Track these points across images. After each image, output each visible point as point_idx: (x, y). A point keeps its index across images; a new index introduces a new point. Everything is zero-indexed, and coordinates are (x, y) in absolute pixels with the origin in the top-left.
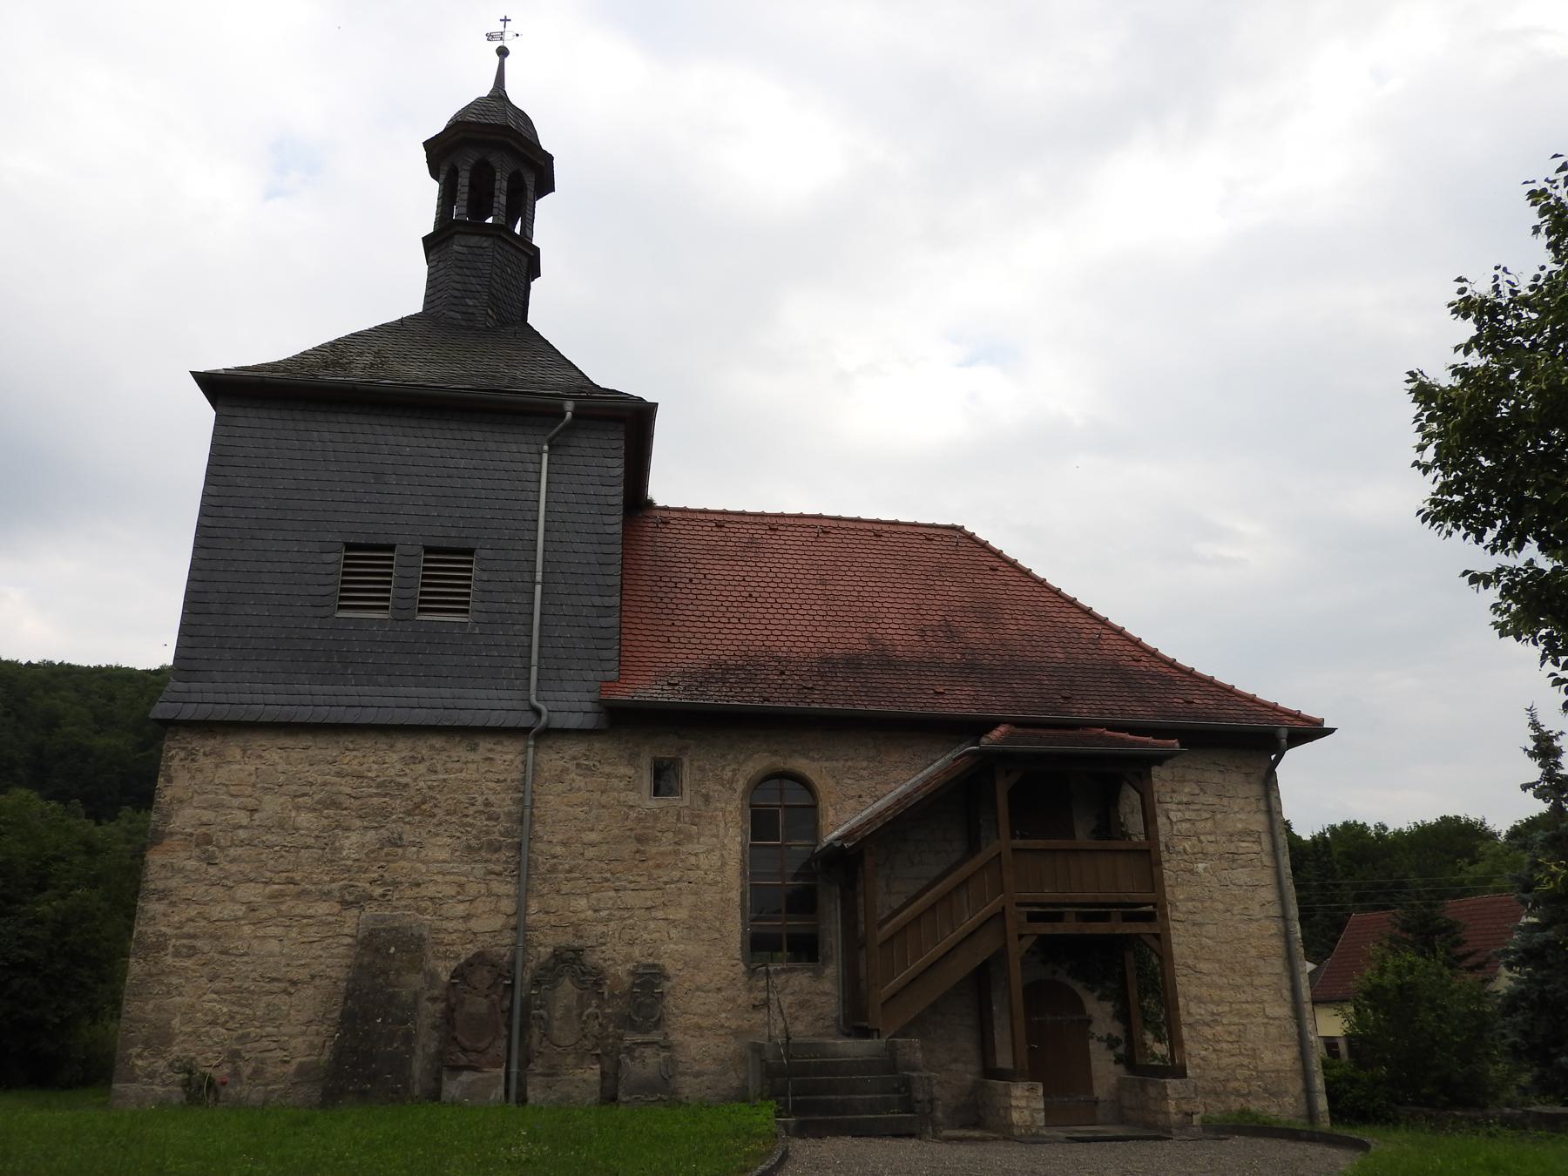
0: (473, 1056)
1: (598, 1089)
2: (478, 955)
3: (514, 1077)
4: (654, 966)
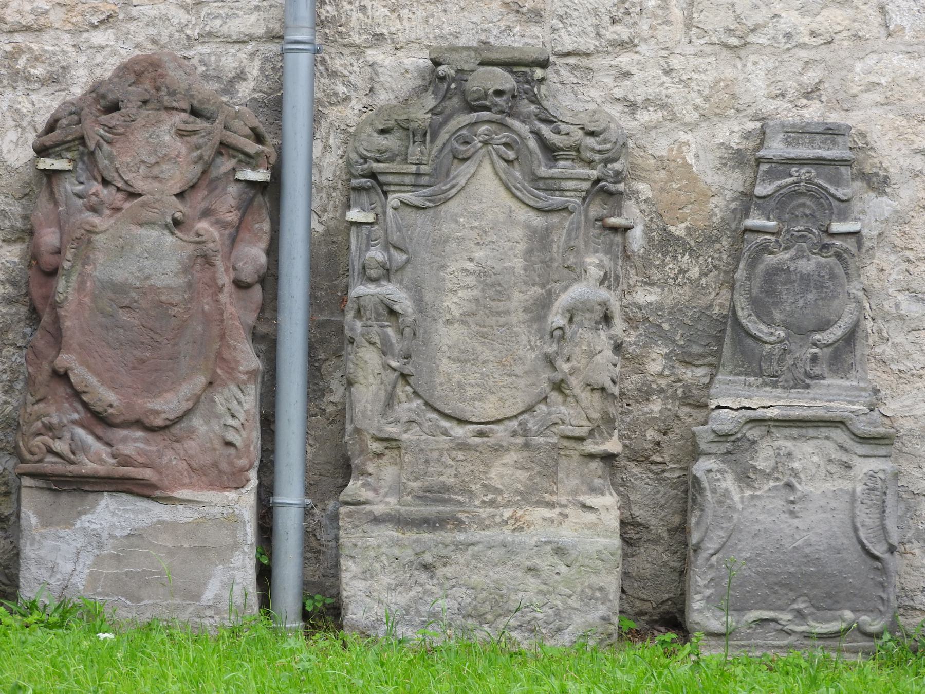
0: (133, 443)
1: (611, 581)
2: (144, 72)
3: (289, 524)
4: (832, 133)
